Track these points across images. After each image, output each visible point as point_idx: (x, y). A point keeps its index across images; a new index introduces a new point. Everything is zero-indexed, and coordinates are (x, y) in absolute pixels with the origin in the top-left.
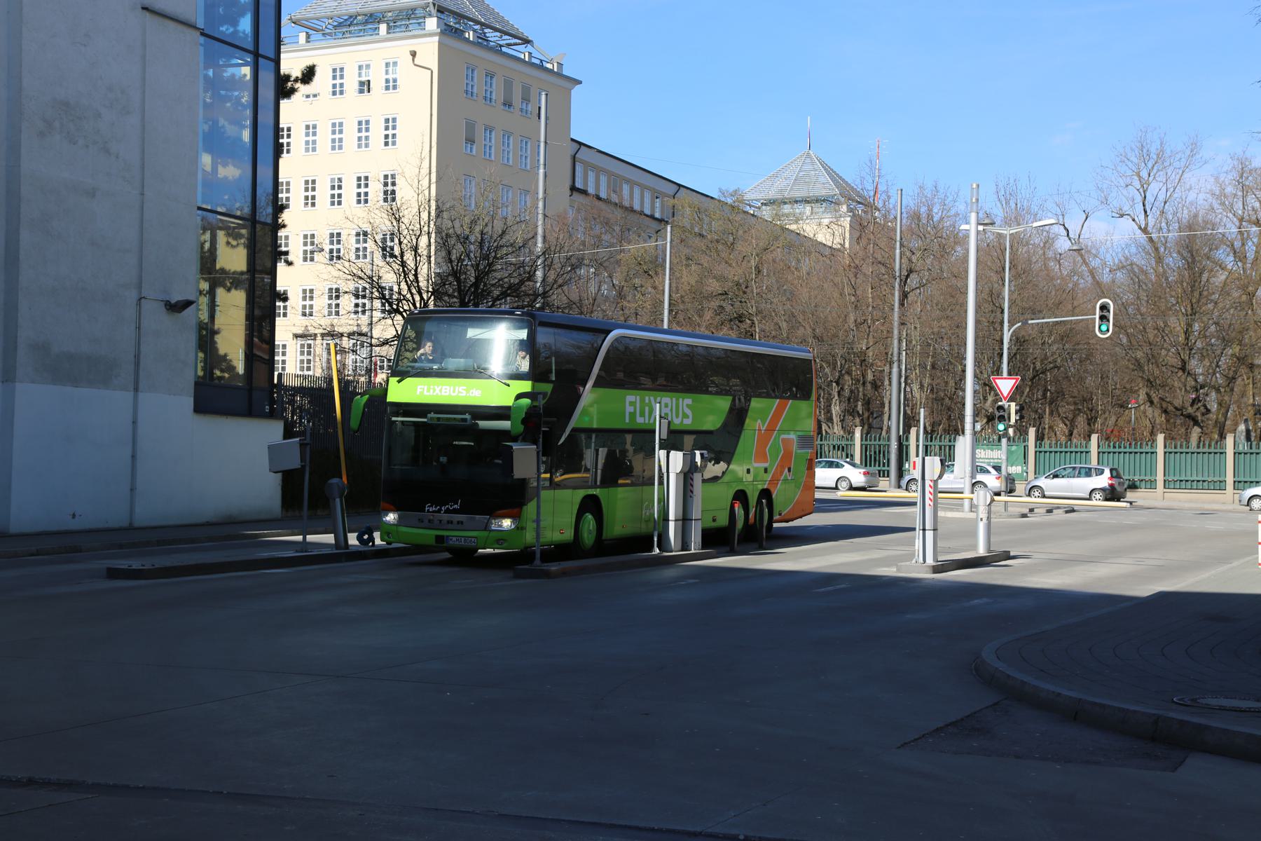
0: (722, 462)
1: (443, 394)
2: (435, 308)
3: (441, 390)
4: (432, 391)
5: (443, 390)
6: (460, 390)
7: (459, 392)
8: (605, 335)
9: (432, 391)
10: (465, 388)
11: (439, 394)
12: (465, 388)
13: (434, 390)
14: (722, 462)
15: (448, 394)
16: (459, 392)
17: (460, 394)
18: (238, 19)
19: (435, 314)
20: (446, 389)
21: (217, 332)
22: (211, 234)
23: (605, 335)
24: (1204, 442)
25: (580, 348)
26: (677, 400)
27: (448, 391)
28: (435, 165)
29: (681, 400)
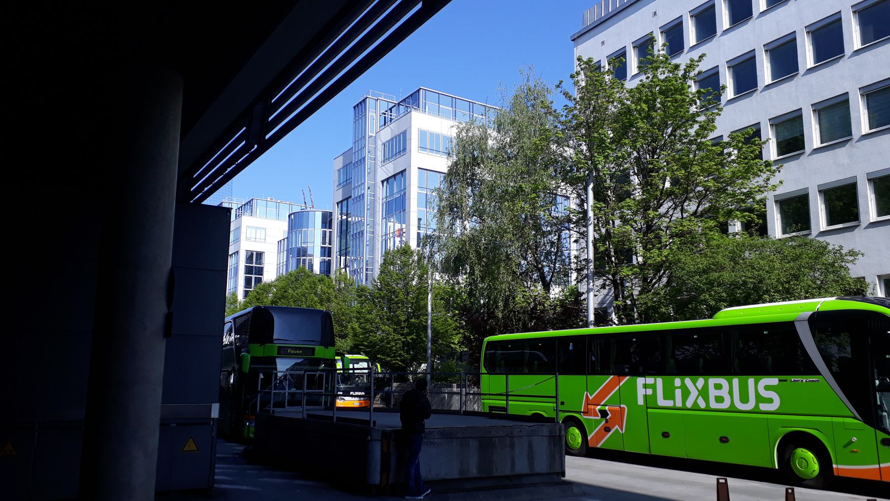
0: (432, 415)
1: (713, 405)
4: (678, 393)
5: (713, 393)
6: (765, 394)
7: (759, 399)
9: (678, 393)
11: (702, 404)
13: (686, 394)
14: (432, 415)
16: (759, 399)
17: (763, 407)
22: (343, 191)
27: (724, 392)
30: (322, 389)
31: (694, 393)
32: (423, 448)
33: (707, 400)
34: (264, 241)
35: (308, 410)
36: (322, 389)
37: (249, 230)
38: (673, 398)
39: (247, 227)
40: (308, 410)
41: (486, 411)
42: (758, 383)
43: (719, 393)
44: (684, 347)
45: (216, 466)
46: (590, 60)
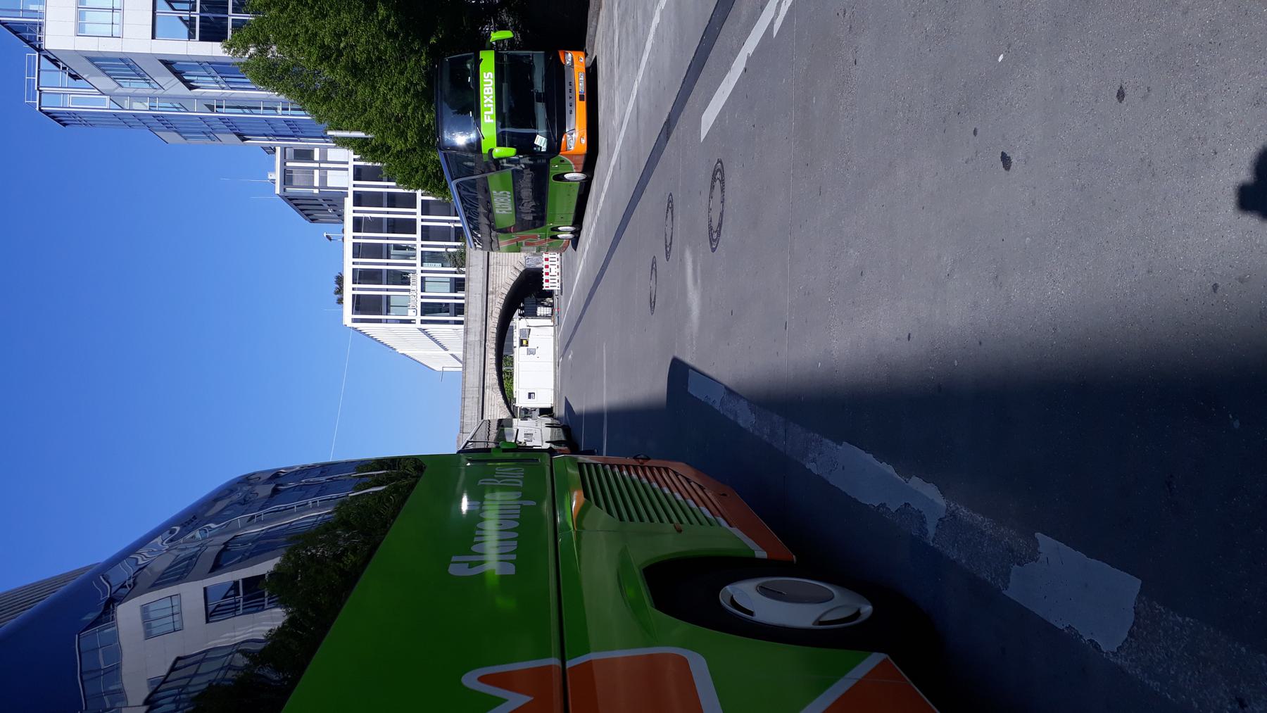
0: (487, 152)
2: (585, 99)
3: (488, 96)
4: (489, 105)
5: (488, 93)
6: (488, 76)
7: (489, 78)
8: (690, 370)
9: (489, 105)
10: (485, 74)
12: (485, 74)
13: (489, 103)
15: (491, 89)
16: (489, 78)
18: (511, 569)
19: (105, 61)
20: (486, 91)
21: (498, 547)
22: (529, 703)
23: (690, 370)
24: (626, 28)
25: (230, 667)
26: (484, 83)
27: (488, 89)
28: (503, 670)
29: (485, 80)
30: (423, 227)
31: (488, 100)
33: (490, 95)
34: (116, 14)
35: (375, 225)
36: (423, 227)
37: (89, 29)
38: (490, 108)
39: (80, 31)
40: (375, 225)
41: (516, 544)
42: (512, 563)
43: (488, 91)
45: (461, 369)
46: (482, 520)
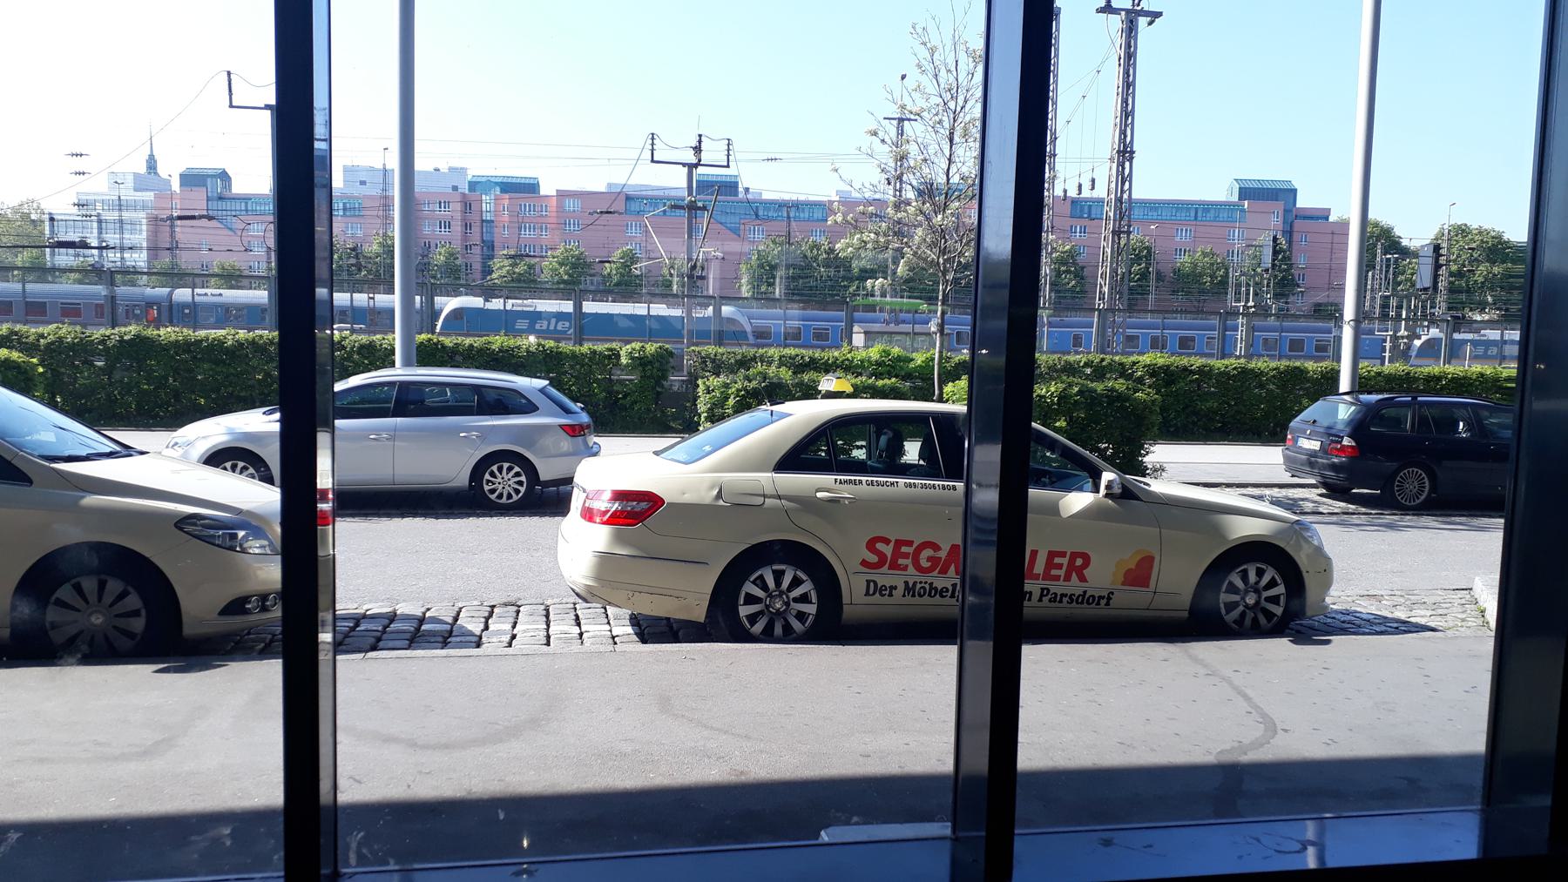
28: (630, 305)
32: (1551, 745)
43: (1433, 311)
44: (857, 443)
